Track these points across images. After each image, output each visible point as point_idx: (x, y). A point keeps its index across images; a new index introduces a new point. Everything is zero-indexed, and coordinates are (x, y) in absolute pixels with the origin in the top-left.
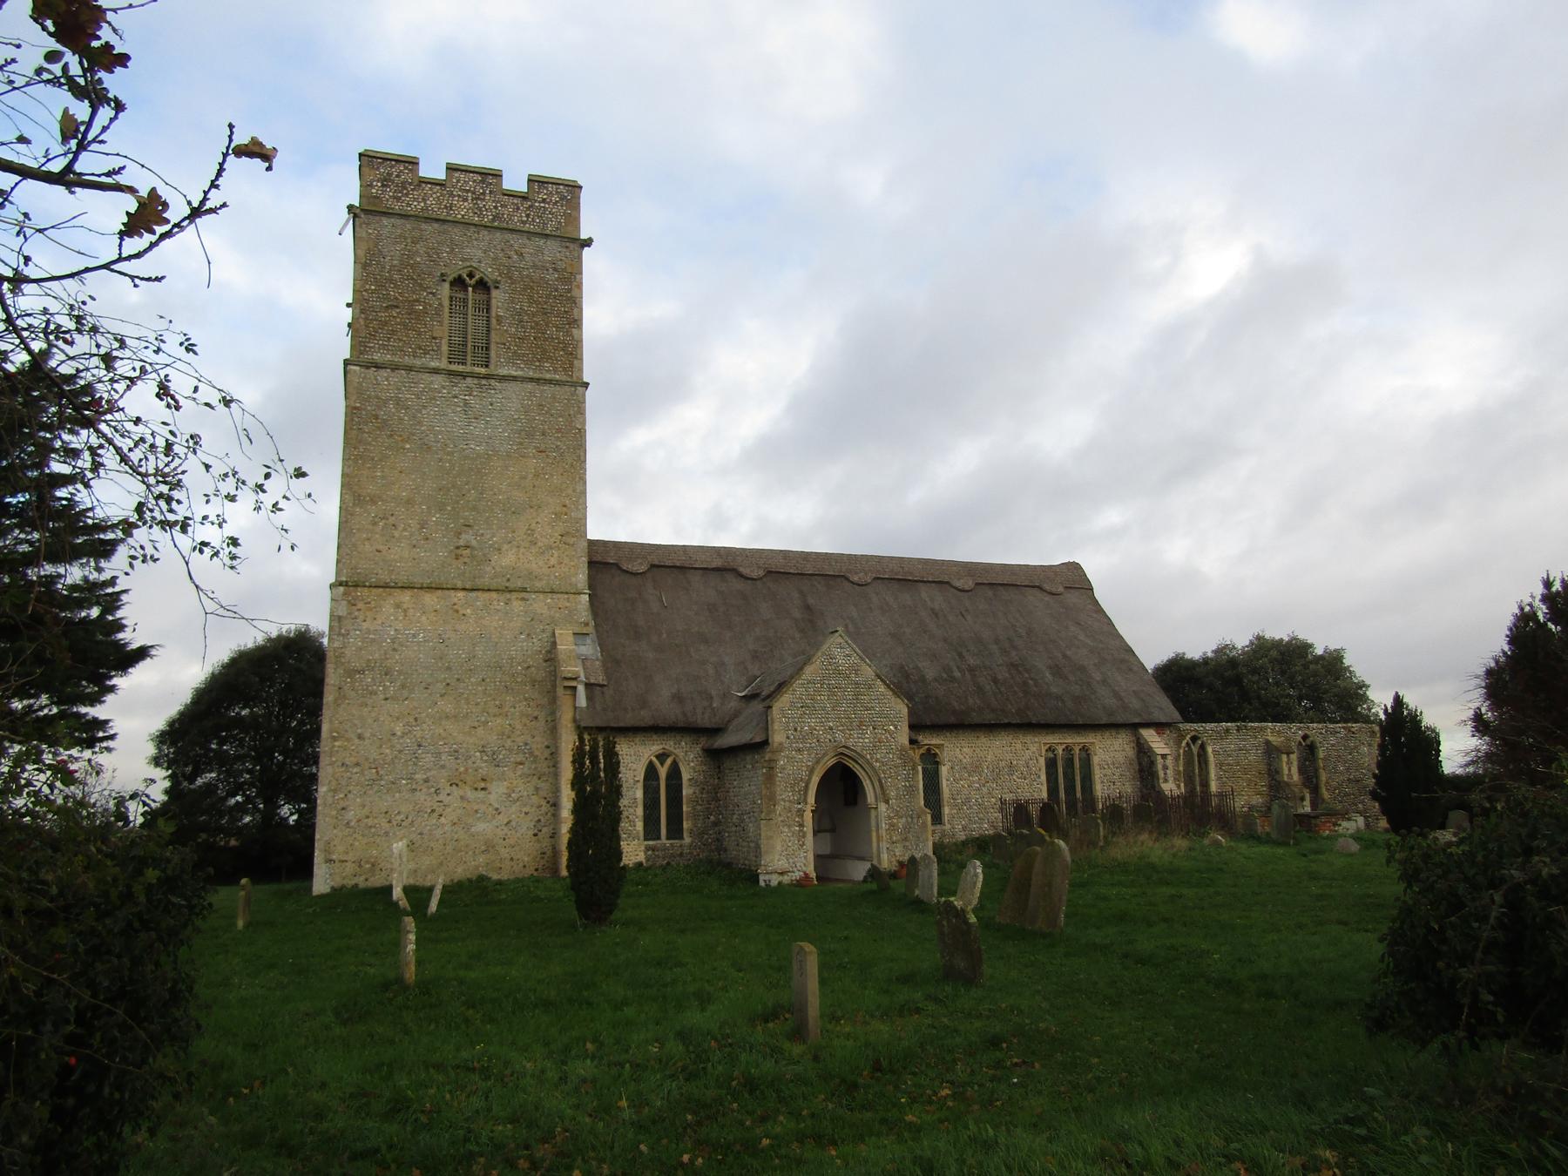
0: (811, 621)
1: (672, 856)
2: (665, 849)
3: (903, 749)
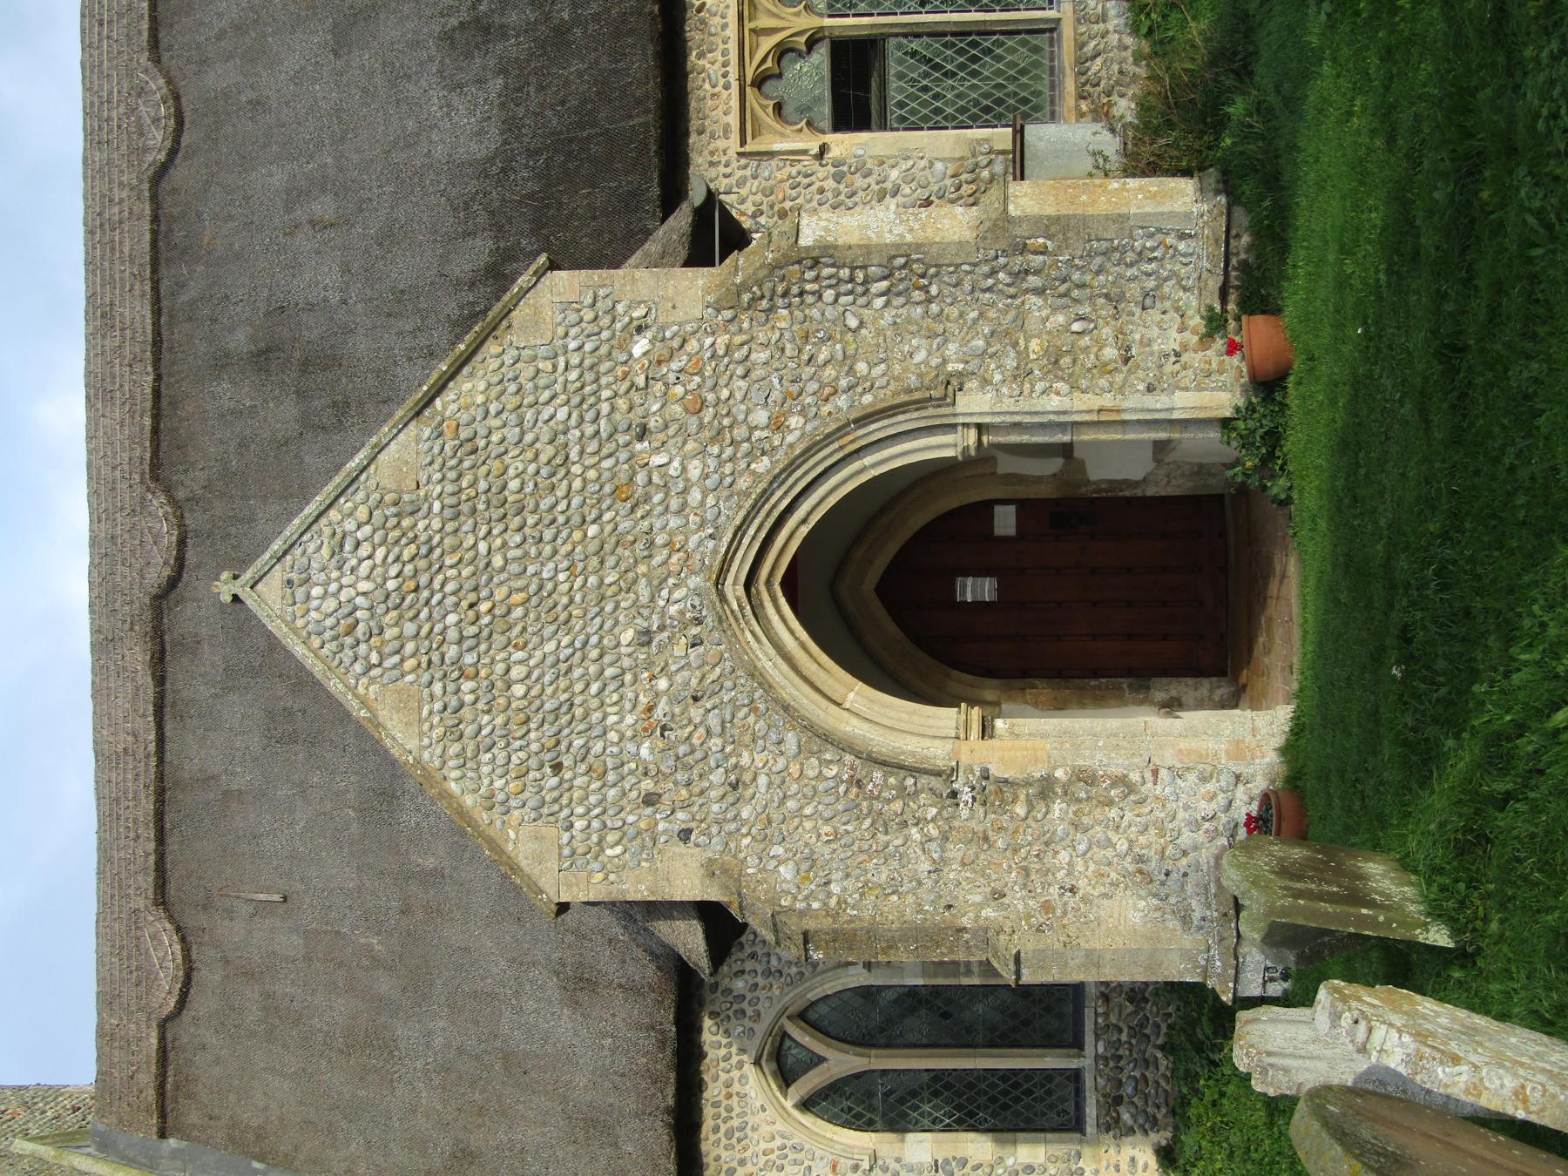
0: (305, 366)
1: (1137, 1032)
2: (1111, 1059)
3: (731, 301)
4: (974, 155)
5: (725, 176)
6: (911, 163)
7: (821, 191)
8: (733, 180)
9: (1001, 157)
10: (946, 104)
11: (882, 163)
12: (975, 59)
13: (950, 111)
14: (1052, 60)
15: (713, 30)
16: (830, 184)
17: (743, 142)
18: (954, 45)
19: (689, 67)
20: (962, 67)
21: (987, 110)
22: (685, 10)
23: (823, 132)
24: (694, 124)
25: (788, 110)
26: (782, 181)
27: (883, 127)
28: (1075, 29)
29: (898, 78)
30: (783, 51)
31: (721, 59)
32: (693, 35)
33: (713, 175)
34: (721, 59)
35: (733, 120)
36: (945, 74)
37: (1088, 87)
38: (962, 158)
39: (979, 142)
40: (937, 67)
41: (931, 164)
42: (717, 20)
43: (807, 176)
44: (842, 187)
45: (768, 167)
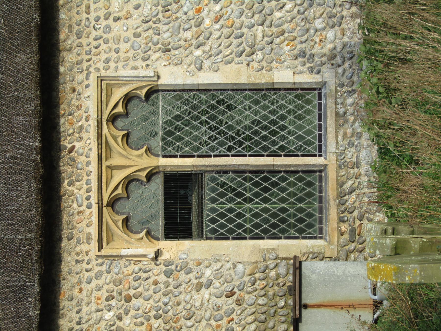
4: (265, 260)
5: (87, 270)
6: (220, 265)
7: (156, 283)
8: (92, 274)
9: (284, 262)
10: (245, 221)
11: (199, 264)
12: (266, 190)
13: (248, 226)
14: (321, 192)
15: (80, 166)
16: (162, 278)
17: (100, 248)
18: (252, 179)
19: (62, 191)
20: (257, 195)
21: (274, 226)
22: (60, 151)
23: (158, 239)
24: (65, 233)
25: (133, 222)
26: (128, 275)
27: (201, 237)
28: (338, 172)
29: (209, 204)
30: (129, 181)
31: (85, 187)
32: (65, 169)
33: (79, 270)
34: (85, 187)
35: (93, 231)
36: (245, 200)
37: (346, 214)
38: (256, 262)
39: (269, 251)
40: (239, 195)
41: (234, 266)
42: (83, 159)
43: (145, 272)
44: (170, 280)
45: (117, 266)
